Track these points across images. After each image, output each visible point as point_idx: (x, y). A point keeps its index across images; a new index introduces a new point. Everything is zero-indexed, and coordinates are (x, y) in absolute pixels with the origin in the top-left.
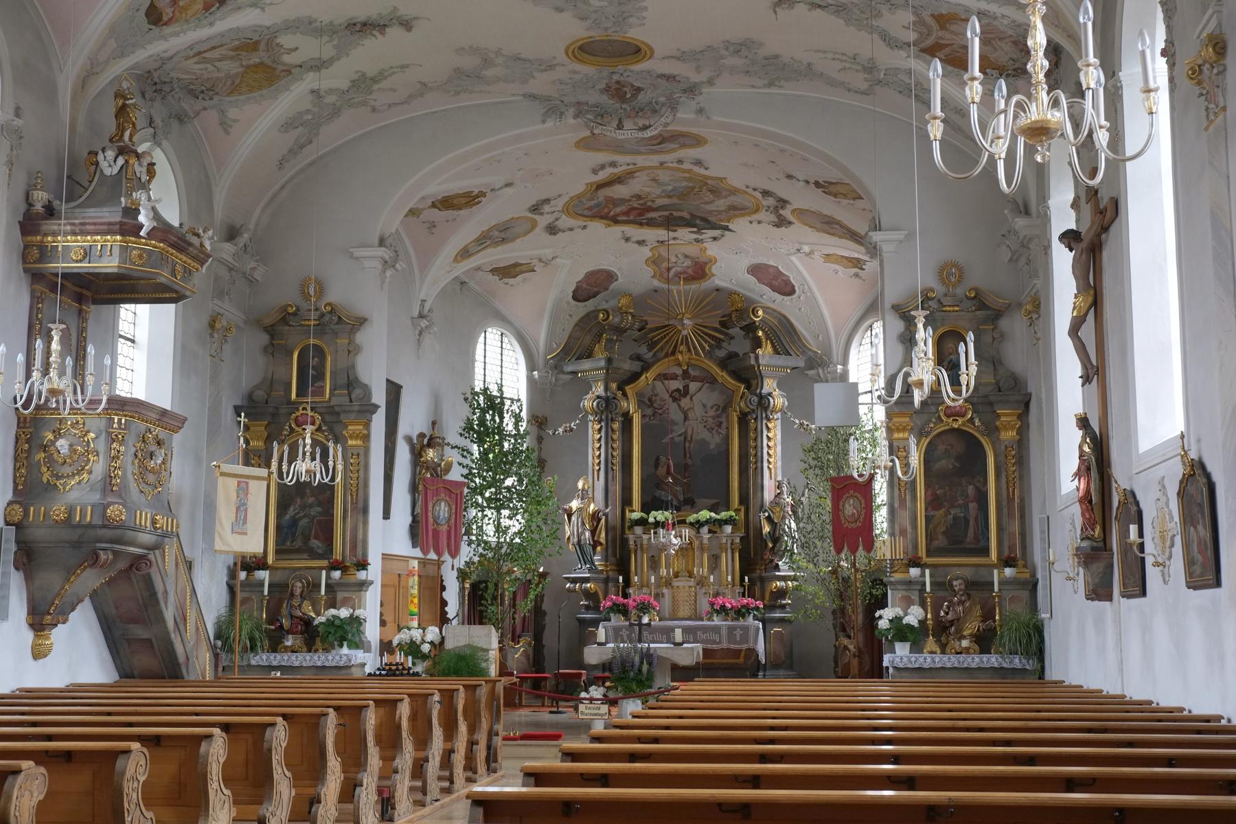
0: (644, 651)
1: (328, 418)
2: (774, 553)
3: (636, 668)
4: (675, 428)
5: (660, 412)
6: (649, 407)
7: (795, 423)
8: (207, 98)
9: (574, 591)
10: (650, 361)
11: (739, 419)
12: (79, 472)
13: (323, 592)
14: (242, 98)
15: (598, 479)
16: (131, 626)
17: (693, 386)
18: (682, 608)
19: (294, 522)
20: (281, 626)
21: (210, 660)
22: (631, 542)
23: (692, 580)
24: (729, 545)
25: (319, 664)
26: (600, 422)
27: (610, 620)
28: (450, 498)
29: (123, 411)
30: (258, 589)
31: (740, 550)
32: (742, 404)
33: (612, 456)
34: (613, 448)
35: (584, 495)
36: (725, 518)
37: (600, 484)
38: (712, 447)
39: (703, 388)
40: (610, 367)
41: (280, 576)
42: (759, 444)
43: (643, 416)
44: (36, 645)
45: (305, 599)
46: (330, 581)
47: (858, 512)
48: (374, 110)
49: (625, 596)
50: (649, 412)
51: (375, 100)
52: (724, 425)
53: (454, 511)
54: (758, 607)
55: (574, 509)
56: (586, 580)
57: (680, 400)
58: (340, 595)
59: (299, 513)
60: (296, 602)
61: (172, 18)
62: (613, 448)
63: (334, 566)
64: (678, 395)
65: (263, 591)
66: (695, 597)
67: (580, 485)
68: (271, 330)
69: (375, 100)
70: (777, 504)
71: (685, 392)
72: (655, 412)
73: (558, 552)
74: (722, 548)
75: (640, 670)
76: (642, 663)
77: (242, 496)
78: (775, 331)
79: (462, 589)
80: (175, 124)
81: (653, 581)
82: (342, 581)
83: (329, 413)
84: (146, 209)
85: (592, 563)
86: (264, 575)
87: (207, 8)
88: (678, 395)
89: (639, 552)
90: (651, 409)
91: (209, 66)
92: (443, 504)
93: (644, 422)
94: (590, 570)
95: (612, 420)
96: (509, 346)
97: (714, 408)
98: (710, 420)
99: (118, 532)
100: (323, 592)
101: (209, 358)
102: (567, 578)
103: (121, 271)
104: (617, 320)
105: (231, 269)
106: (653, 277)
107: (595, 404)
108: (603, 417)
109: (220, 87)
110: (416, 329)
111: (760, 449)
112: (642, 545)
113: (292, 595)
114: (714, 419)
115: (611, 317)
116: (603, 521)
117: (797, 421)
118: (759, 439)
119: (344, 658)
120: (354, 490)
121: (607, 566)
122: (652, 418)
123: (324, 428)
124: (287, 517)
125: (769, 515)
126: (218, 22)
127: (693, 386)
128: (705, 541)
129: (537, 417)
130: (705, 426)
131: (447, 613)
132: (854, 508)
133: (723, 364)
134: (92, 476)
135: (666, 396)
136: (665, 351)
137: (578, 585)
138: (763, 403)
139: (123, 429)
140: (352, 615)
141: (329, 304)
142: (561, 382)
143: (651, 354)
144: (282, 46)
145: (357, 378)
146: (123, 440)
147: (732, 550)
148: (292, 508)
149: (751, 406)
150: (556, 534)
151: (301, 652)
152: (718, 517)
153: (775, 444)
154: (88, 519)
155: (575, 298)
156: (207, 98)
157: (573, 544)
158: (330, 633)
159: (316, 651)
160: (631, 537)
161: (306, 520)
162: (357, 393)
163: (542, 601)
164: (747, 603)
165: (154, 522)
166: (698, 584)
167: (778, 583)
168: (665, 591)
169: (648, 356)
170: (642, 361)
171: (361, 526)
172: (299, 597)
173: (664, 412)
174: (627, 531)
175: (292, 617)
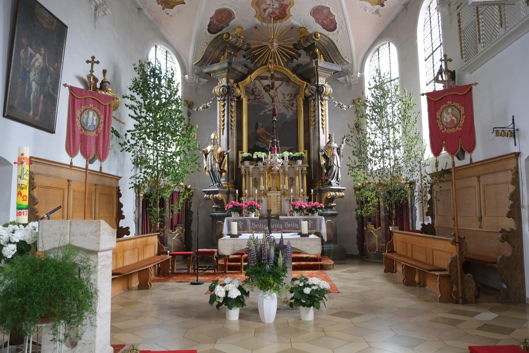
0: (278, 242)
2: (327, 176)
3: (272, 261)
4: (267, 106)
5: (258, 97)
6: (252, 95)
7: (336, 104)
9: (209, 199)
10: (252, 68)
11: (304, 102)
15: (223, 135)
17: (277, 83)
18: (273, 208)
22: (243, 171)
23: (279, 192)
24: (300, 172)
26: (224, 101)
27: (231, 216)
28: (99, 108)
32: (307, 91)
33: (231, 121)
34: (231, 116)
35: (215, 142)
36: (298, 156)
37: (224, 137)
38: (288, 117)
39: (283, 84)
40: (230, 67)
42: (317, 114)
43: (249, 100)
47: (457, 118)
49: (240, 201)
50: (252, 97)
52: (295, 105)
53: (102, 120)
54: (322, 207)
55: (209, 151)
56: (216, 192)
57: (269, 91)
62: (231, 116)
64: (268, 88)
66: (281, 202)
67: (212, 136)
70: (329, 147)
71: (272, 87)
72: (255, 98)
73: (198, 170)
74: (296, 173)
75: (276, 263)
76: (277, 255)
78: (325, 49)
79: (138, 197)
81: (256, 192)
85: (220, 182)
88: (268, 88)
89: (247, 176)
90: (253, 96)
92: (91, 113)
93: (249, 103)
94: (218, 186)
95: (231, 100)
96: (171, 60)
97: (289, 96)
98: (287, 102)
102: (205, 192)
104: (234, 40)
106: (255, 16)
107: (221, 90)
108: (226, 98)
110: (91, 3)
111: (317, 117)
112: (249, 172)
114: (289, 102)
115: (231, 38)
116: (226, 158)
117: (337, 103)
121: (228, 185)
122: (254, 101)
127: (277, 83)
128: (287, 169)
129: (187, 101)
131: (122, 212)
132: (453, 115)
133: (294, 71)
135: (262, 89)
136: (261, 63)
137: (211, 195)
138: (319, 90)
142: (201, 84)
143: (253, 65)
147: (302, 174)
149: (312, 92)
150: (196, 161)
152: (295, 155)
153: (326, 114)
155: (209, 31)
157: (208, 171)
160: (243, 167)
163: (190, 206)
164: (316, 205)
166: (282, 195)
167: (331, 193)
168: (263, 199)
169: (251, 66)
170: (248, 68)
173: (260, 98)
174: (240, 164)
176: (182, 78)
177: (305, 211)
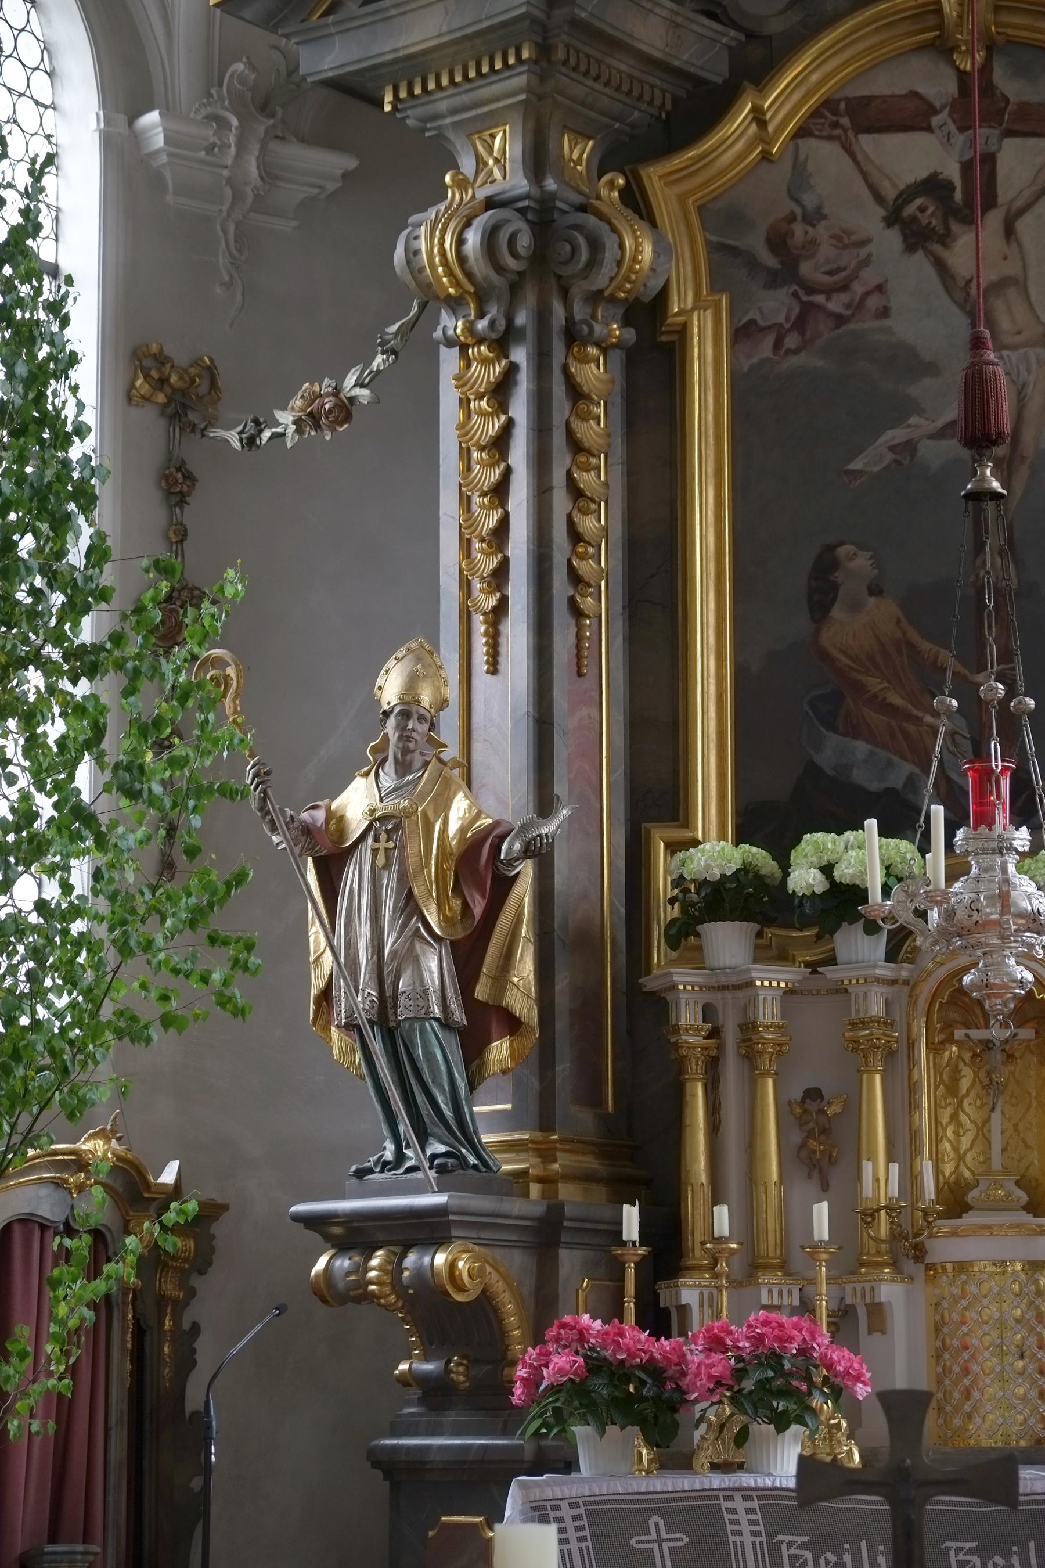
5: (836, 304)
6: (774, 280)
15: (494, 668)
26: (501, 344)
27: (569, 1465)
33: (575, 536)
34: (576, 492)
57: (945, 239)
62: (576, 492)
73: (224, 1001)
81: (822, 1229)
89: (731, 1068)
95: (572, 336)
102: (315, 1222)
107: (473, 238)
108: (521, 319)
112: (748, 1028)
121: (546, 1154)
122: (791, 341)
129: (162, 359)
157: (351, 1027)
174: (659, 952)
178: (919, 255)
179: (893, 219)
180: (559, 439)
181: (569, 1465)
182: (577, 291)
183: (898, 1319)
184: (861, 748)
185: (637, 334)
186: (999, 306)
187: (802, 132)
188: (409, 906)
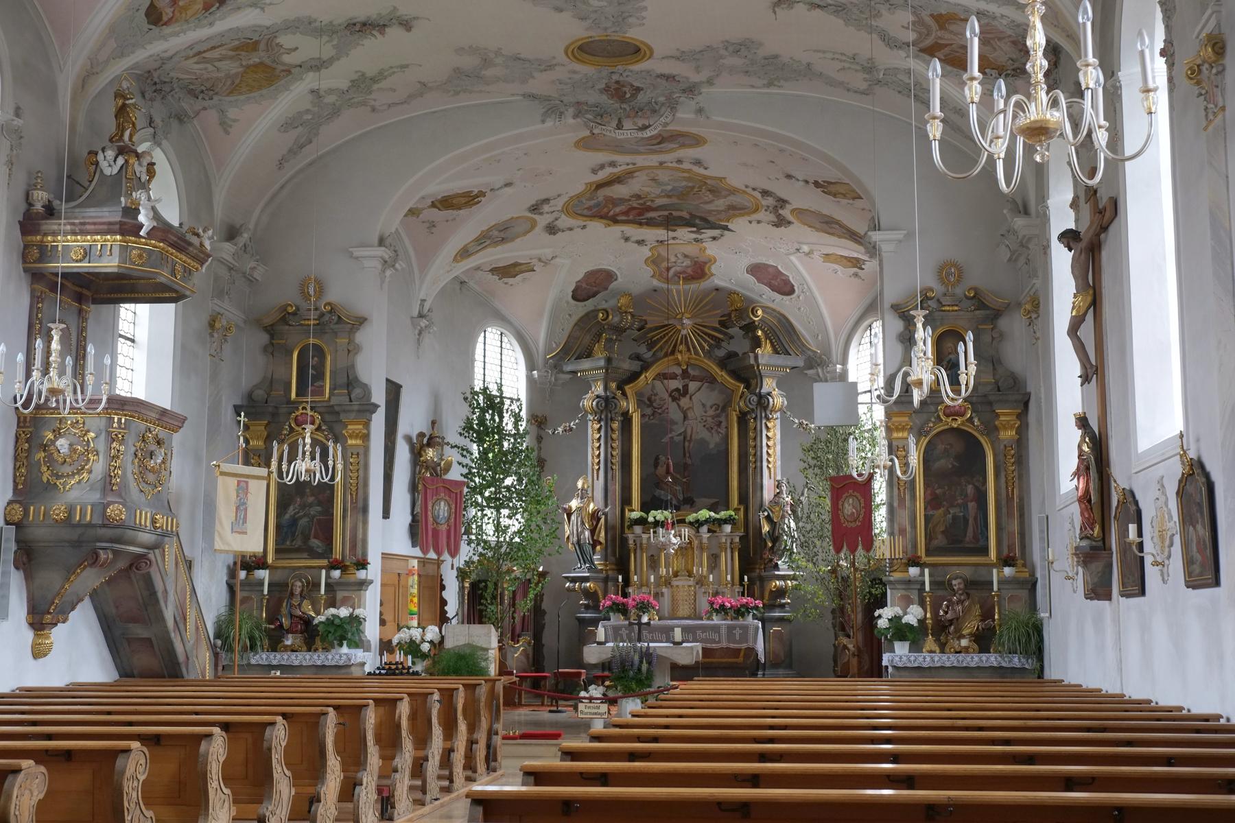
0: (644, 650)
1: (328, 418)
2: (773, 553)
3: (636, 667)
4: (675, 427)
5: (659, 411)
6: (649, 406)
7: (795, 423)
8: (207, 98)
9: (574, 590)
10: (649, 360)
11: (739, 418)
12: (79, 472)
13: (323, 591)
14: (242, 97)
15: (598, 479)
16: (131, 625)
17: (693, 386)
18: (681, 607)
19: (294, 521)
20: (281, 626)
21: (209, 659)
22: (631, 542)
23: (692, 579)
24: (728, 544)
25: (319, 663)
26: (599, 422)
27: (610, 620)
28: (450, 497)
29: (123, 410)
30: (258, 588)
31: (739, 549)
33: (612, 455)
34: (612, 447)
35: (583, 495)
36: (724, 517)
38: (712, 446)
39: (703, 388)
41: (279, 575)
42: (759, 444)
43: (643, 416)
44: (36, 644)
45: (305, 598)
46: (330, 581)
47: (857, 511)
48: (374, 110)
49: (625, 595)
50: (649, 411)
51: (375, 100)
52: (724, 424)
53: (453, 510)
54: (758, 607)
55: (574, 508)
56: (585, 579)
57: (679, 400)
58: (340, 595)
59: (298, 512)
60: (295, 602)
61: (172, 18)
62: (612, 447)
63: (334, 566)
64: (677, 395)
65: (263, 591)
66: (695, 596)
67: (580, 484)
68: (270, 330)
69: (375, 100)
70: (777, 503)
71: (685, 391)
72: (655, 412)
73: (558, 552)
74: (722, 547)
75: (640, 669)
76: (641, 662)
77: (241, 496)
78: (774, 331)
80: (175, 124)
81: (652, 580)
82: (342, 580)
83: (329, 413)
84: (146, 209)
85: (592, 562)
86: (263, 574)
87: (207, 8)
88: (677, 395)
89: (638, 551)
90: (650, 409)
91: (208, 66)
92: (442, 503)
93: (643, 422)
94: (589, 569)
95: (612, 419)
97: (714, 408)
98: (709, 419)
99: (118, 531)
100: (323, 591)
101: (209, 358)
102: (567, 578)
103: (121, 271)
105: (230, 269)
106: (652, 277)
107: (594, 403)
108: (603, 417)
109: (220, 86)
110: (415, 328)
111: (759, 449)
112: (641, 544)
113: (292, 594)
114: (713, 419)
115: (610, 317)
116: (602, 520)
117: (797, 421)
118: (759, 438)
119: (344, 657)
120: (354, 489)
121: (606, 565)
122: (652, 418)
123: (324, 428)
124: (287, 516)
125: (769, 515)
126: (218, 22)
127: (693, 386)
128: (705, 541)
129: (537, 416)
130: (704, 426)
131: (446, 612)
133: (722, 363)
134: (92, 476)
135: (666, 396)
136: (665, 350)
137: (577, 584)
138: (763, 402)
139: (122, 429)
140: (351, 615)
141: (329, 304)
142: (560, 382)
143: (651, 353)
144: (281, 46)
145: (356, 377)
146: (123, 439)
147: (732, 549)
148: (291, 508)
149: (750, 406)
151: (301, 651)
152: (718, 516)
153: (775, 444)
154: (88, 518)
155: (575, 297)
156: (207, 98)
157: (573, 544)
158: (330, 632)
159: (316, 650)
160: (631, 536)
161: (305, 520)
162: (357, 392)
164: (747, 603)
165: (154, 521)
166: (697, 584)
167: (778, 582)
168: (664, 590)
169: (648, 355)
170: (642, 361)
171: (360, 525)
172: (299, 596)
173: (663, 411)
174: (626, 531)
175: (292, 616)
176: (527, 376)
177: (732, 613)
178: (675, 403)
179: (670, 395)
180: (609, 438)
181: (610, 620)
182: (613, 412)
183: (666, 595)
184: (663, 492)
185: (581, 652)
186: (688, 412)
187: (654, 379)
188: (583, 523)
